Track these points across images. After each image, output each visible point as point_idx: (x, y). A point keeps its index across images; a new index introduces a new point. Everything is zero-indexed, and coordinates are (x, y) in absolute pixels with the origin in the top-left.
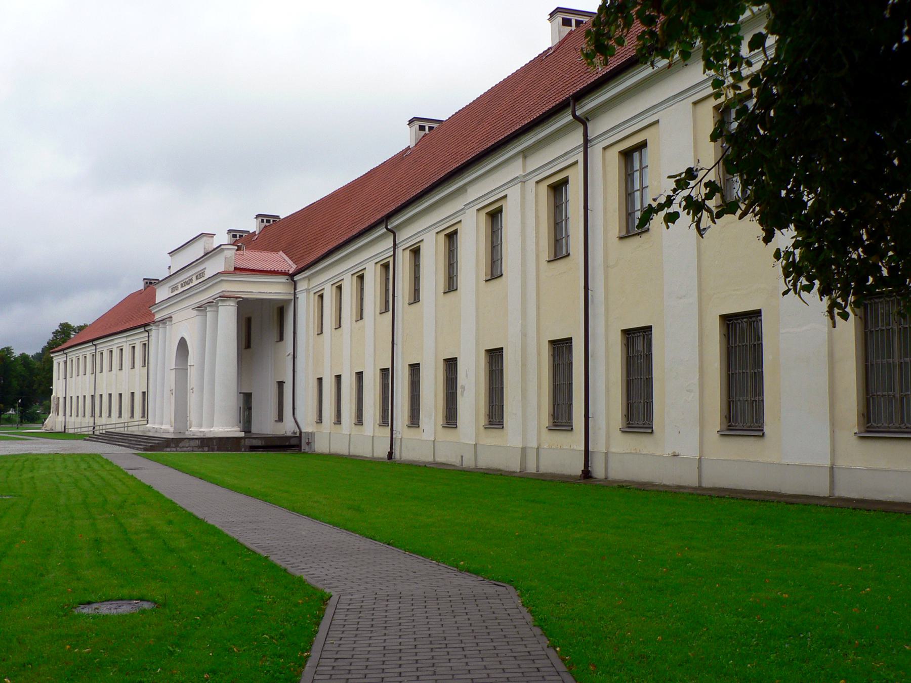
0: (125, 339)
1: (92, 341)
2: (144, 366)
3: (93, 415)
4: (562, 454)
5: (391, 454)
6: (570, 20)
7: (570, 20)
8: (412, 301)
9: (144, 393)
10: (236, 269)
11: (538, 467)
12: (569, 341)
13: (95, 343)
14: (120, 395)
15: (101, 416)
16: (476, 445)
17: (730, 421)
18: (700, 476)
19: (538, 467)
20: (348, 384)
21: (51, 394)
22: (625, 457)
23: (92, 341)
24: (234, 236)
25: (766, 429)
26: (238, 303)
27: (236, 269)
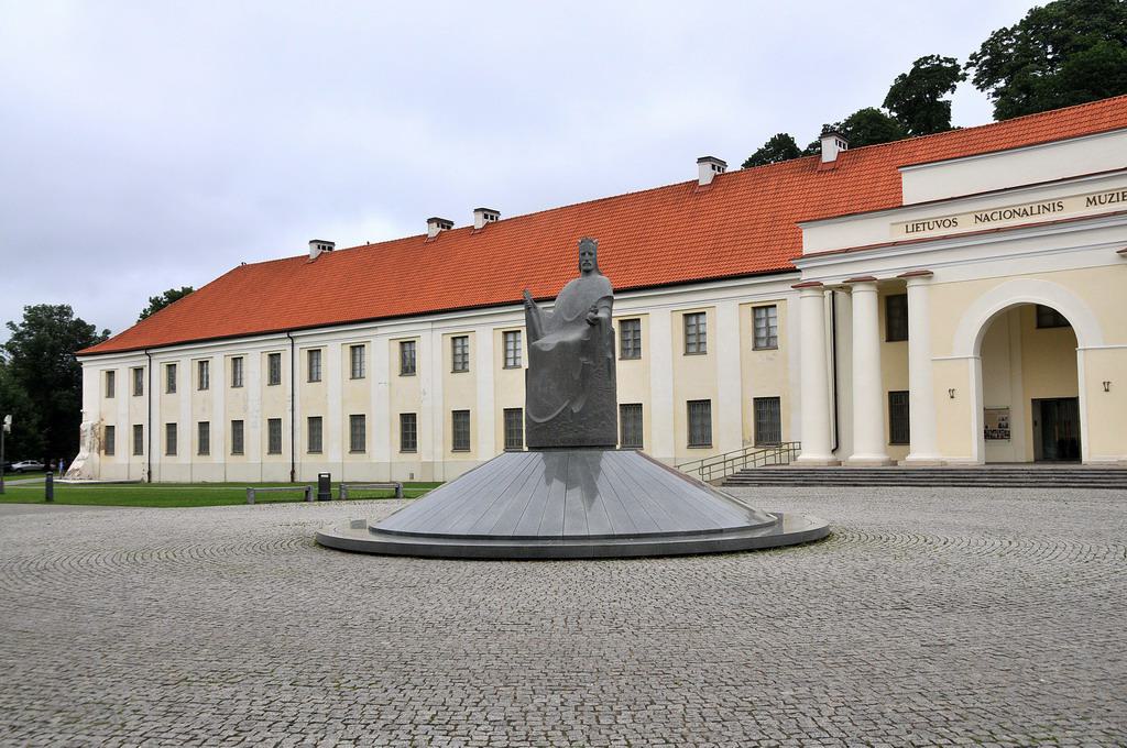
0: (429, 326)
13: (293, 334)
24: (486, 217)
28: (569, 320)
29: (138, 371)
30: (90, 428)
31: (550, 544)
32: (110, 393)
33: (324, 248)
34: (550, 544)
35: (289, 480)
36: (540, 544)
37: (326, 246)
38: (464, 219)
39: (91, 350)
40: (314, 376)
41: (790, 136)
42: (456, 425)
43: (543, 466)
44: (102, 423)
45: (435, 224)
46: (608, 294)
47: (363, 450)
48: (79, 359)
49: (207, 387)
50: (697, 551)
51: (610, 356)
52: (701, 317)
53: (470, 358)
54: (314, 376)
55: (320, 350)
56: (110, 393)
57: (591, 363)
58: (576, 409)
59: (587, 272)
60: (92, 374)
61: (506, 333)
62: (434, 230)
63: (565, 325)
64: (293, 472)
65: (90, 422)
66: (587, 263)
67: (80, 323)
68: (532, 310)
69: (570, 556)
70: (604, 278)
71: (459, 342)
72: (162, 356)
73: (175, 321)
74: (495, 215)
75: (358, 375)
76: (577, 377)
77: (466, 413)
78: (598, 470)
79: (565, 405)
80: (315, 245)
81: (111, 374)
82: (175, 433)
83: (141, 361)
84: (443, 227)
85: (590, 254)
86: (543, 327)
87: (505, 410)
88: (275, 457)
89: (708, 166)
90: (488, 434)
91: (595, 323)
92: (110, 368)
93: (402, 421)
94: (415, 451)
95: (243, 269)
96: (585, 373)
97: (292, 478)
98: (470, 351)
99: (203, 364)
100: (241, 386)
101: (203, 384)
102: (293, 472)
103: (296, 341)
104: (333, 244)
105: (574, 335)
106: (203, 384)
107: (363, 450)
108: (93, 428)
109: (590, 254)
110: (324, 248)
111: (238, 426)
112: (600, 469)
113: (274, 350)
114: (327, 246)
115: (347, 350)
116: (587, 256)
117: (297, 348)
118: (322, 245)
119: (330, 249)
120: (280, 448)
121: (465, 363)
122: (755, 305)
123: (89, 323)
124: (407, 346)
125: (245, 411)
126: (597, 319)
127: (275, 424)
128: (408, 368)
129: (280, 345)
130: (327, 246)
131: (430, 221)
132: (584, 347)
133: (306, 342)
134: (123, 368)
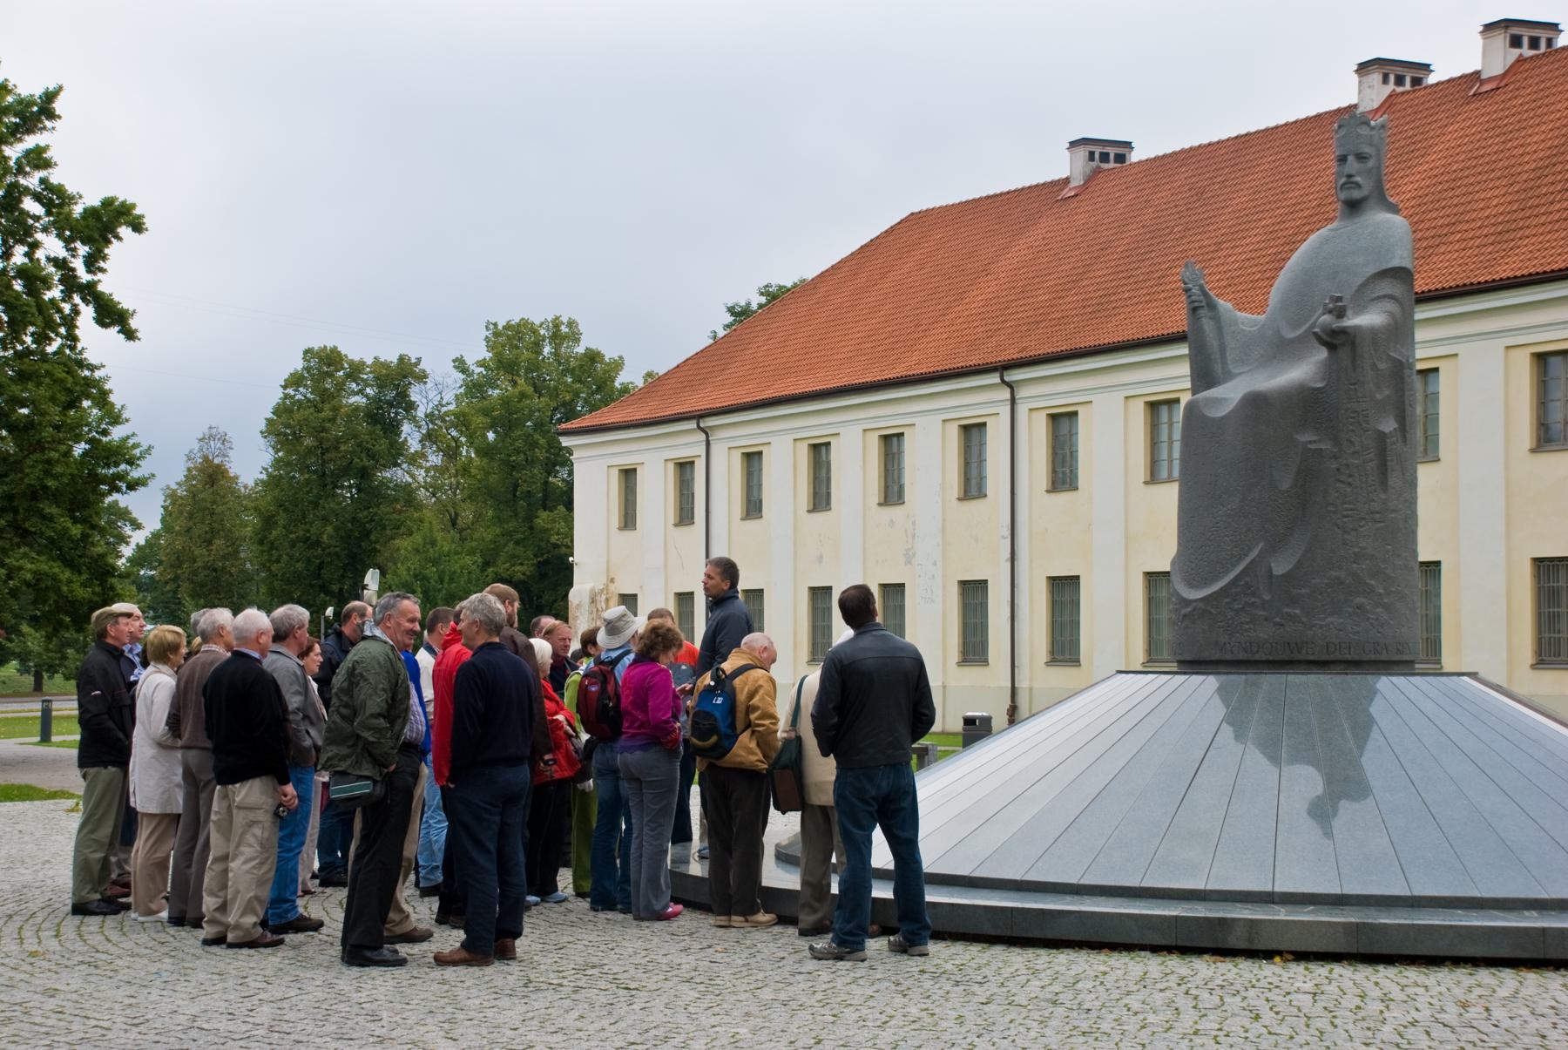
12: (981, 585)
13: (704, 423)
24: (1516, 42)
28: (1290, 335)
29: (684, 468)
30: (586, 600)
31: (1281, 914)
32: (628, 520)
33: (1104, 157)
34: (1281, 914)
36: (1200, 911)
37: (1105, 155)
38: (1456, 54)
39: (574, 424)
40: (1063, 476)
43: (1219, 710)
44: (612, 587)
45: (1376, 77)
46: (1396, 263)
48: (565, 442)
50: (988, 929)
51: (1389, 425)
54: (1063, 476)
55: (1075, 414)
56: (628, 520)
57: (1326, 446)
58: (1280, 567)
59: (1354, 207)
60: (592, 471)
62: (1378, 92)
63: (1281, 350)
65: (588, 586)
66: (1349, 182)
67: (593, 357)
68: (1202, 312)
69: (1377, 949)
70: (1397, 220)
73: (796, 354)
74: (1543, 35)
75: (1164, 474)
76: (1286, 484)
78: (1363, 727)
79: (1253, 555)
80: (1082, 153)
81: (629, 474)
82: (902, 608)
83: (688, 444)
85: (1361, 157)
86: (1230, 356)
88: (973, 674)
90: (1115, 618)
91: (1336, 340)
92: (627, 461)
95: (915, 219)
96: (1310, 472)
99: (819, 451)
103: (1022, 393)
104: (1128, 145)
105: (1302, 371)
108: (593, 601)
109: (1361, 157)
112: (1370, 722)
113: (971, 415)
114: (1112, 151)
115: (1139, 412)
116: (1352, 165)
117: (1022, 409)
118: (1098, 150)
119: (1121, 158)
123: (609, 354)
124: (1062, 423)
125: (909, 562)
126: (1343, 332)
129: (982, 400)
130: (1112, 151)
131: (1364, 68)
132: (1307, 405)
133: (1046, 391)
134: (654, 459)
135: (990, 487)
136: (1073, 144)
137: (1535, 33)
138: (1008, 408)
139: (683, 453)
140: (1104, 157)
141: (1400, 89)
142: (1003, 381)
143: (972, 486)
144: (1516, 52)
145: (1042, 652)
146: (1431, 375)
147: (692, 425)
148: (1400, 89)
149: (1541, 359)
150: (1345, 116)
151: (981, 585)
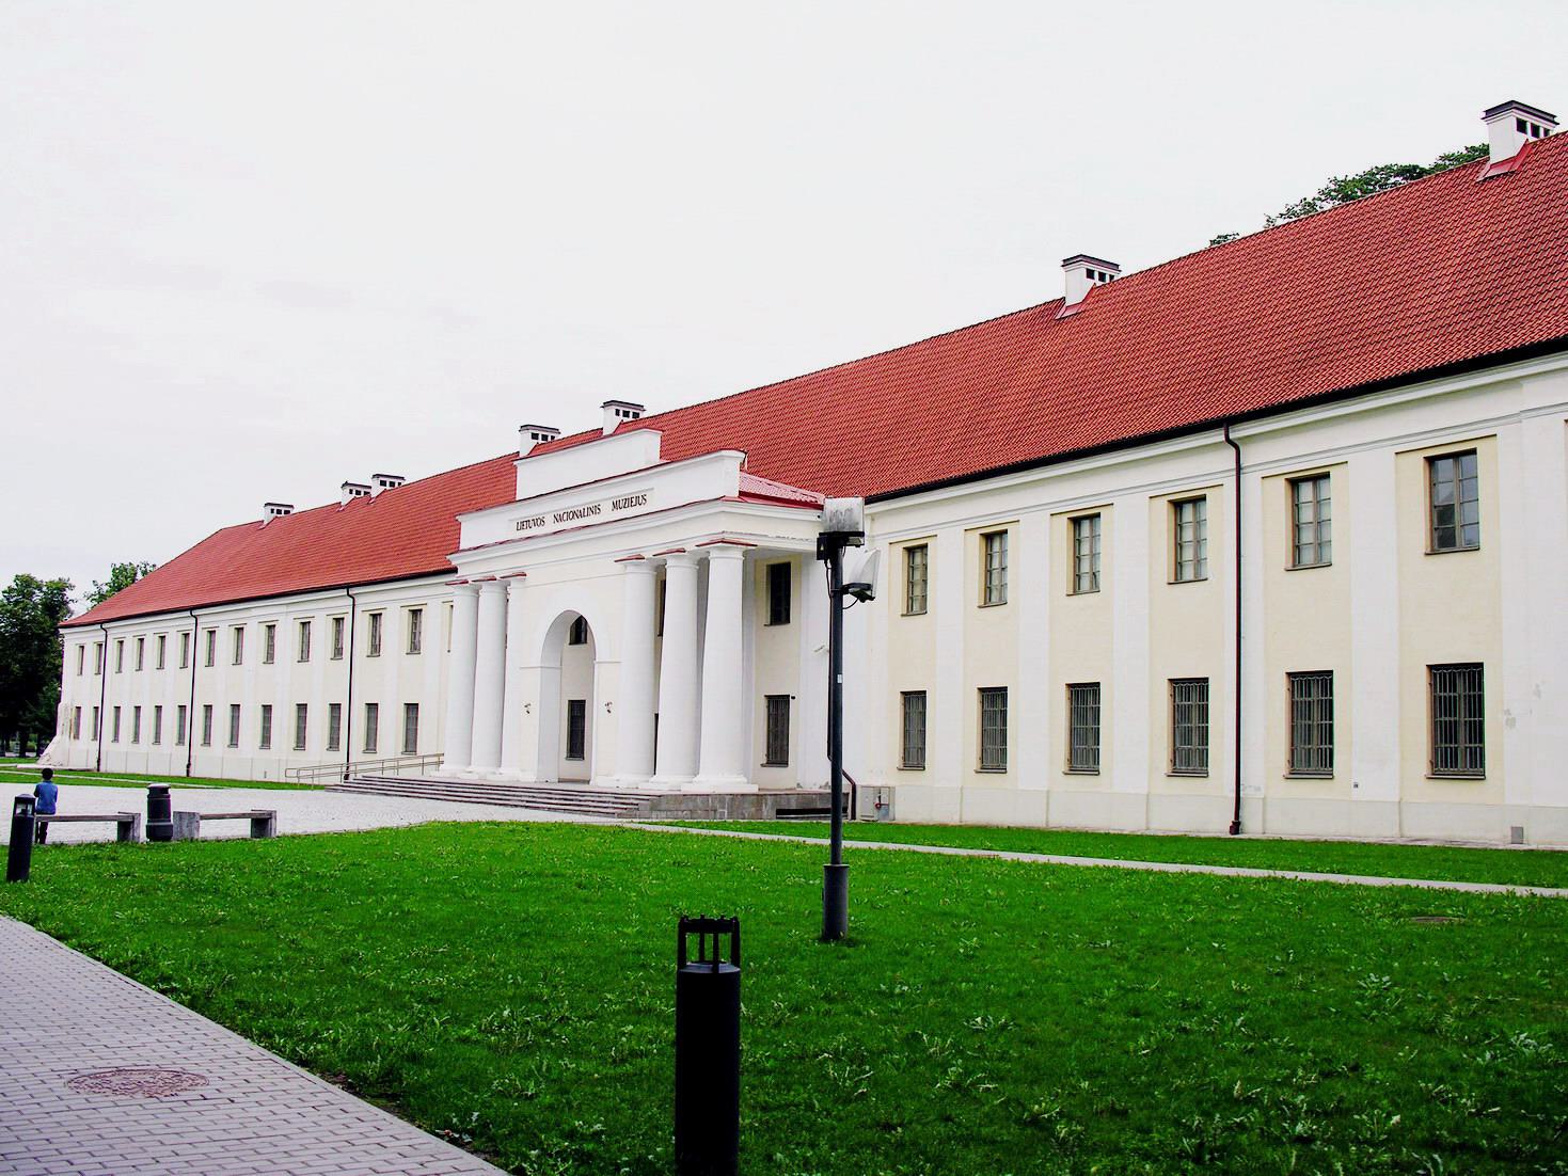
0: (284, 609)
1: (191, 609)
2: (185, 666)
3: (97, 735)
4: (1197, 808)
5: (1236, 827)
6: (624, 416)
7: (624, 416)
8: (1290, 567)
9: (182, 708)
10: (742, 494)
11: (1047, 822)
12: (1201, 684)
13: (195, 613)
14: (267, 709)
15: (207, 741)
16: (1048, 792)
17: (1175, 765)
18: (1147, 823)
19: (1047, 822)
20: (148, 716)
21: (58, 700)
22: (1290, 809)
23: (348, 586)
24: (535, 436)
25: (1486, 774)
26: (745, 554)
27: (742, 494)
35: (185, 774)
37: (280, 510)
41: (32, 575)
42: (1180, 714)
47: (784, 763)
48: (448, 557)
49: (1095, 587)
52: (1323, 484)
53: (1335, 533)
61: (1295, 483)
64: (189, 766)
71: (1306, 491)
72: (137, 628)
77: (1094, 688)
84: (626, 414)
87: (1430, 667)
89: (1080, 271)
92: (415, 603)
93: (1433, 685)
94: (1481, 777)
97: (188, 772)
98: (1333, 511)
100: (1322, 564)
101: (1084, 578)
102: (189, 766)
106: (1084, 578)
107: (784, 763)
110: (279, 512)
111: (994, 699)
114: (283, 509)
118: (276, 508)
120: (1096, 760)
121: (1321, 545)
122: (303, 621)
124: (1450, 464)
127: (1190, 694)
128: (1448, 530)
129: (1197, 464)
135: (1209, 570)
136: (1067, 262)
137: (359, 489)
138: (1235, 478)
139: (338, 612)
140: (279, 512)
141: (626, 420)
142: (1228, 440)
143: (1184, 568)
144: (383, 488)
145: (363, 746)
146: (1465, 459)
147: (99, 626)
148: (626, 420)
149: (1431, 461)
150: (257, 526)
151: (1201, 684)
